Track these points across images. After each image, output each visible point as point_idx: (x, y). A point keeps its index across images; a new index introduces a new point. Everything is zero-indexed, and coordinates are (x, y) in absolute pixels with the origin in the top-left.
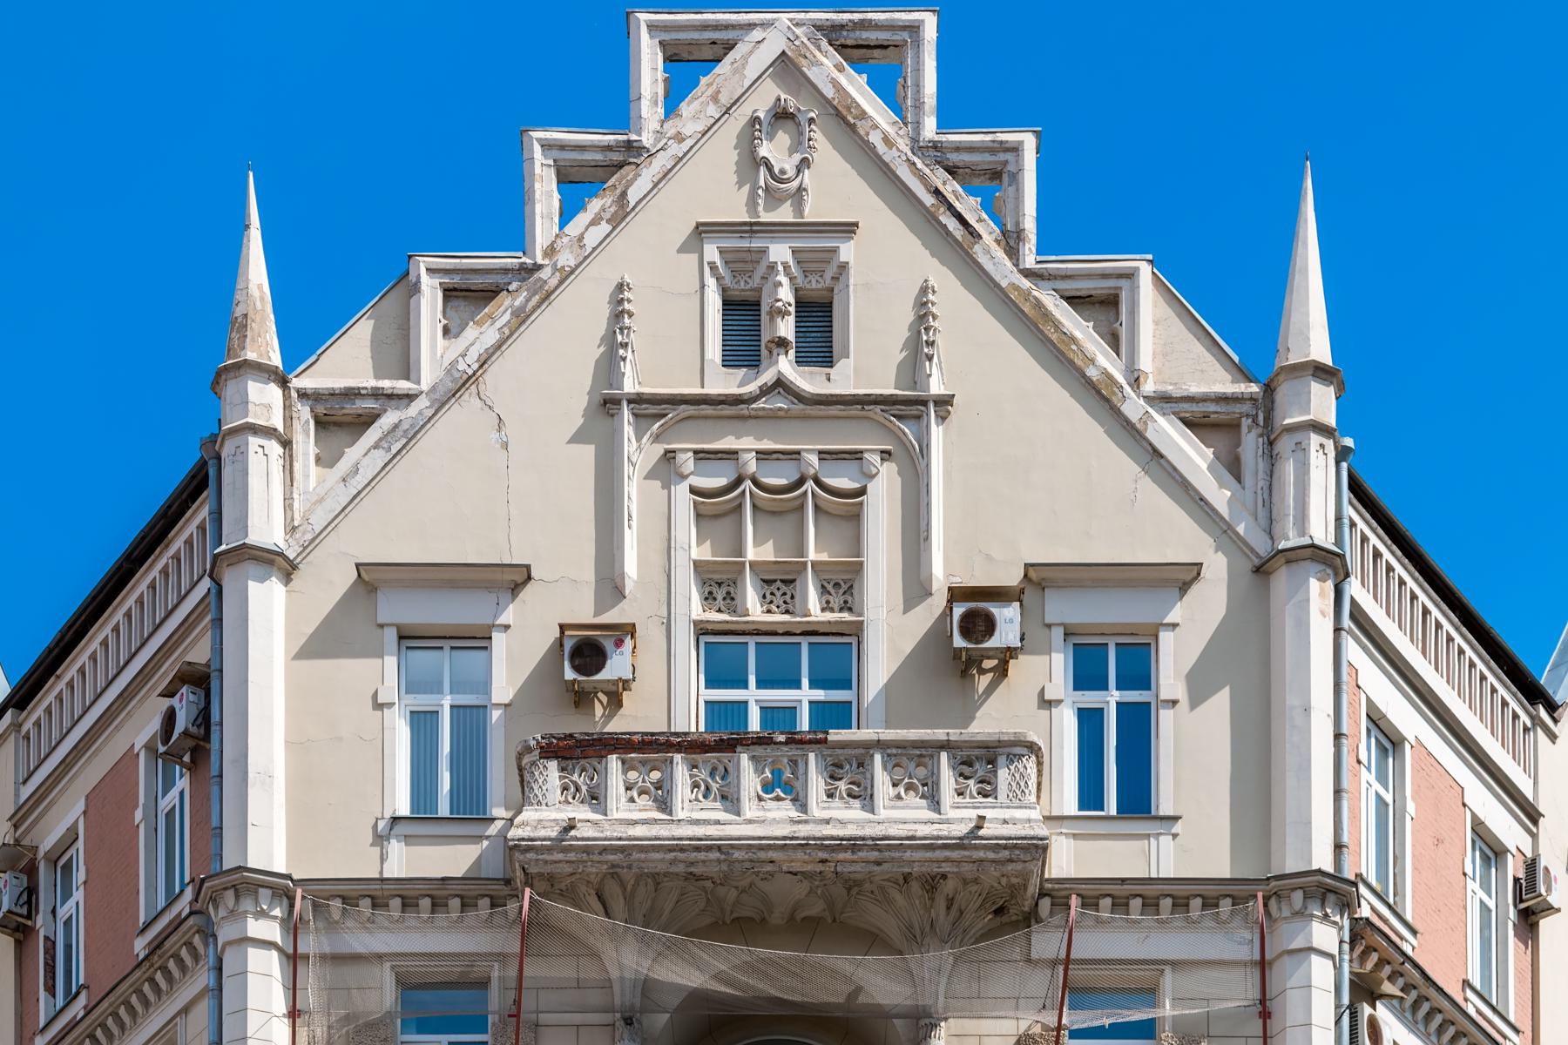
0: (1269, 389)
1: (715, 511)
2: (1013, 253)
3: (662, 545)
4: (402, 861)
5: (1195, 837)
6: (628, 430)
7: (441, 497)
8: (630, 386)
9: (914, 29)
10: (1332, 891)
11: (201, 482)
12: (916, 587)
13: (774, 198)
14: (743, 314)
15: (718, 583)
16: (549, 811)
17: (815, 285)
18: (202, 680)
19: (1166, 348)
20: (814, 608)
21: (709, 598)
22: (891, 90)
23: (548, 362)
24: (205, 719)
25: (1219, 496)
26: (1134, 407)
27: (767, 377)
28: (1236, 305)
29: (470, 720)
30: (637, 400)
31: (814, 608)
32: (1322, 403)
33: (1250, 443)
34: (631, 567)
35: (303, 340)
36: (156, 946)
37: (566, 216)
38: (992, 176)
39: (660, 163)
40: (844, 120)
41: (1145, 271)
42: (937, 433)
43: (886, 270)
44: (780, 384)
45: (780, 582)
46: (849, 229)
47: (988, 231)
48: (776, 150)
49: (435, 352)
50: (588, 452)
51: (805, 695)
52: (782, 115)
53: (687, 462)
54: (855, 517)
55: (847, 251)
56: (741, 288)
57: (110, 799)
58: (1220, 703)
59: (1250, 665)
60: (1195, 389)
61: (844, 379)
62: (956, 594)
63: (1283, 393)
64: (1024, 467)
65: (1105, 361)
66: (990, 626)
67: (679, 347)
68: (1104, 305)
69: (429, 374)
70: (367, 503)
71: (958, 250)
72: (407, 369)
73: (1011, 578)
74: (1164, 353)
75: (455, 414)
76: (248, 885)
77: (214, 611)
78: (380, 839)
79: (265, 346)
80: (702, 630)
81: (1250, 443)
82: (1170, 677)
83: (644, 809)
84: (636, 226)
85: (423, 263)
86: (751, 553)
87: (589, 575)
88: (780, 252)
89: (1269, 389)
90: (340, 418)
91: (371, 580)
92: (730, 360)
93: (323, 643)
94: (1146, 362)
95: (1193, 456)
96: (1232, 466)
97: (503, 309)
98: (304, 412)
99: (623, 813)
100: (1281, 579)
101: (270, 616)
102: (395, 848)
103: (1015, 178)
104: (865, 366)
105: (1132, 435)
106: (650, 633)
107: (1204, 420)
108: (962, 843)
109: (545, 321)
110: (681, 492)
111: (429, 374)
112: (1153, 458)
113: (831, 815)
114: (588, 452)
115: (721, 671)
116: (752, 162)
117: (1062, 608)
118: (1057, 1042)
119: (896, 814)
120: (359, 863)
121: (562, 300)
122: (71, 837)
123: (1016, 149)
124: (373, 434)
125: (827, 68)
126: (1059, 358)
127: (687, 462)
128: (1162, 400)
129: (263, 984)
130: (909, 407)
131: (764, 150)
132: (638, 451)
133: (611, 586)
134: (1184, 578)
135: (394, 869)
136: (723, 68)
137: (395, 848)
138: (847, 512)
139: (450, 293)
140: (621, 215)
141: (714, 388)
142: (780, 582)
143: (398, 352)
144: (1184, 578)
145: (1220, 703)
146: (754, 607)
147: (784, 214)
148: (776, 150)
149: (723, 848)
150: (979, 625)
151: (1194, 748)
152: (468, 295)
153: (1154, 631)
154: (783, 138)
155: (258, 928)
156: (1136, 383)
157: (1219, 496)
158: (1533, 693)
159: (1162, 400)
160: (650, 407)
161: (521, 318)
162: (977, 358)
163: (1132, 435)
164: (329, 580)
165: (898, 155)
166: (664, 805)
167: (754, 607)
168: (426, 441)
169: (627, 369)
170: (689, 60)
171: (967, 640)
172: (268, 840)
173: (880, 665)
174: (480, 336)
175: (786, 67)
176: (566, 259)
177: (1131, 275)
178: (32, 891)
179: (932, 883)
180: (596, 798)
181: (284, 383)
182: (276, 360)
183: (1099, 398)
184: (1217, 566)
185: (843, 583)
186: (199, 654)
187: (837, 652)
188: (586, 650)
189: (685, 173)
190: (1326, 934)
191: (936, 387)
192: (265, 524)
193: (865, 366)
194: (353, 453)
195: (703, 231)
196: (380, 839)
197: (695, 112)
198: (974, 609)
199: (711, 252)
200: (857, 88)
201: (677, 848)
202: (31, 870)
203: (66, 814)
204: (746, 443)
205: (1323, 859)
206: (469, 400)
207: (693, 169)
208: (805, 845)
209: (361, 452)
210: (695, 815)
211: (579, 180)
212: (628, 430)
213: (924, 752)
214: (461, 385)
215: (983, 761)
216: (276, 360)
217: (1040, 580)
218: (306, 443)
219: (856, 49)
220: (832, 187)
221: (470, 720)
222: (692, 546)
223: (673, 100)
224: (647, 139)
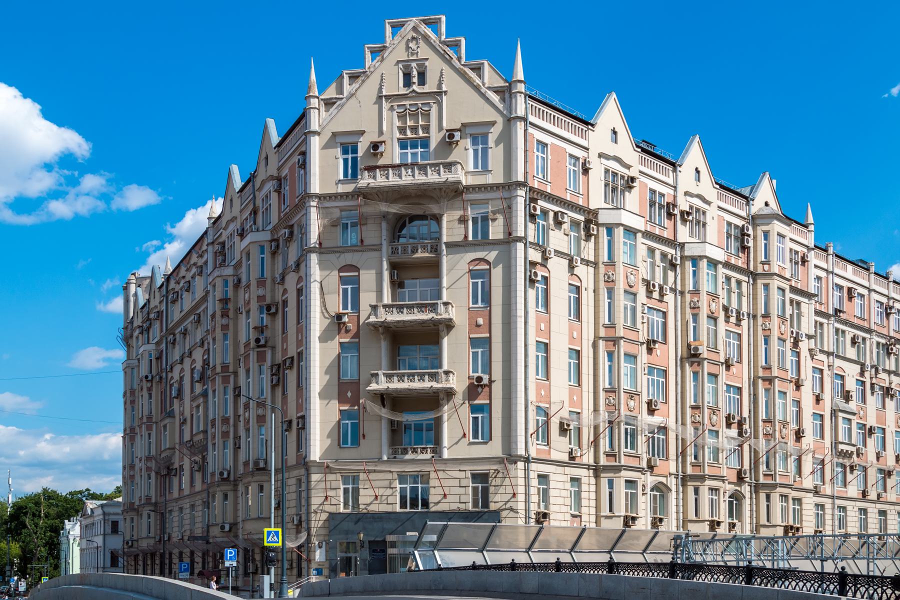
0: (510, 84)
1: (402, 117)
2: (460, 61)
3: (391, 122)
4: (341, 189)
5: (496, 177)
6: (384, 102)
7: (346, 120)
8: (384, 93)
9: (440, 19)
10: (523, 184)
11: (304, 116)
12: (440, 128)
13: (412, 54)
14: (407, 76)
15: (402, 130)
16: (365, 180)
17: (421, 70)
18: (304, 154)
19: (490, 77)
20: (421, 134)
21: (400, 133)
22: (437, 32)
23: (368, 90)
24: (304, 161)
25: (501, 106)
26: (483, 90)
27: (411, 90)
28: (505, 67)
29: (355, 160)
30: (385, 96)
31: (421, 134)
32: (521, 87)
33: (507, 95)
34: (385, 128)
35: (321, 90)
36: (299, 201)
37: (372, 60)
38: (456, 45)
39: (390, 49)
40: (426, 38)
41: (486, 63)
42: (444, 98)
43: (434, 66)
44: (414, 91)
45: (414, 129)
46: (427, 59)
47: (454, 57)
48: (412, 45)
49: (347, 88)
50: (377, 106)
51: (420, 150)
52: (413, 38)
53: (396, 107)
54: (429, 115)
55: (427, 63)
56: (407, 72)
57: (292, 169)
58: (501, 146)
59: (507, 139)
60: (496, 85)
61: (426, 89)
62: (447, 131)
63: (513, 85)
64: (460, 105)
65: (478, 81)
66: (453, 136)
67: (395, 85)
68: (478, 70)
69: (346, 94)
70: (334, 120)
71: (449, 62)
72: (342, 93)
73: (458, 126)
74: (490, 78)
75: (351, 101)
76: (311, 196)
77: (305, 142)
78: (337, 184)
79: (315, 92)
80: (399, 139)
81: (507, 95)
82: (491, 142)
83: (384, 179)
84: (385, 62)
85: (345, 72)
86: (408, 124)
87: (377, 130)
88: (414, 65)
89: (510, 84)
90: (329, 103)
91: (334, 135)
92: (404, 86)
93: (326, 147)
94: (486, 81)
95: (495, 98)
96: (503, 100)
97: (360, 80)
98: (322, 103)
99: (380, 180)
100: (512, 122)
101: (315, 143)
102: (340, 185)
103: (460, 46)
104: (430, 86)
105: (483, 96)
106: (388, 142)
107: (497, 91)
108: (444, 182)
109: (368, 81)
110: (395, 113)
111: (346, 94)
112: (487, 100)
113: (420, 178)
114: (377, 106)
115: (403, 146)
116: (408, 48)
117: (469, 131)
118: (2, 593)
119: (432, 177)
120: (332, 190)
121: (371, 78)
122: (286, 176)
123: (460, 41)
124: (335, 106)
125: (424, 28)
126: (469, 81)
127: (396, 107)
128: (489, 88)
129: (314, 214)
130: (438, 94)
131: (410, 45)
132: (386, 105)
133: (381, 133)
134: (493, 123)
135: (340, 191)
136: (403, 29)
137: (340, 185)
138: (427, 115)
139: (350, 77)
140: (382, 60)
141: (400, 93)
142: (414, 129)
143: (340, 90)
144: (493, 123)
145: (501, 146)
146: (409, 134)
147: (415, 57)
148: (412, 45)
149: (399, 186)
150: (451, 136)
151: (496, 155)
152: (353, 78)
153: (488, 133)
154: (414, 42)
155: (313, 204)
156: (484, 85)
157: (501, 106)
158: (587, 123)
159: (489, 88)
160: (388, 97)
161: (363, 81)
162: (452, 83)
163: (483, 96)
164: (327, 135)
165: (437, 43)
166: (387, 178)
167: (409, 134)
168: (345, 107)
169: (384, 90)
170: (396, 27)
171: (449, 141)
172: (316, 187)
173: (433, 144)
174: (356, 86)
175: (415, 29)
176: (372, 69)
177: (483, 64)
178: (281, 184)
179: (441, 189)
180: (375, 177)
181: (318, 98)
182: (317, 94)
183: (477, 88)
184: (500, 120)
185: (426, 129)
186: (303, 149)
187: (425, 143)
188: (375, 146)
189: (395, 51)
190: (521, 192)
191: (444, 89)
192: (314, 126)
193: (430, 86)
194: (331, 110)
195: (398, 62)
196: (337, 184)
197: (397, 39)
198: (451, 133)
199: (400, 66)
200: (429, 31)
201: (389, 187)
202: (280, 180)
203: (285, 172)
204: (407, 103)
205: (521, 178)
206: (354, 98)
207: (397, 51)
208: (414, 185)
209: (333, 110)
210: (393, 180)
211: (374, 52)
212: (384, 102)
213: (438, 165)
214: (352, 95)
215: (449, 166)
216: (317, 94)
217: (464, 125)
218: (323, 109)
219: (427, 23)
220: (424, 51)
221: (355, 160)
222: (397, 123)
223: (394, 34)
224: (387, 45)
